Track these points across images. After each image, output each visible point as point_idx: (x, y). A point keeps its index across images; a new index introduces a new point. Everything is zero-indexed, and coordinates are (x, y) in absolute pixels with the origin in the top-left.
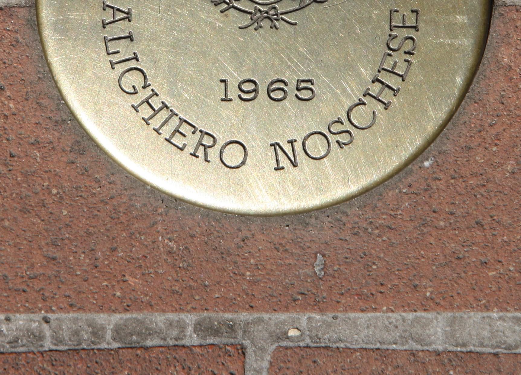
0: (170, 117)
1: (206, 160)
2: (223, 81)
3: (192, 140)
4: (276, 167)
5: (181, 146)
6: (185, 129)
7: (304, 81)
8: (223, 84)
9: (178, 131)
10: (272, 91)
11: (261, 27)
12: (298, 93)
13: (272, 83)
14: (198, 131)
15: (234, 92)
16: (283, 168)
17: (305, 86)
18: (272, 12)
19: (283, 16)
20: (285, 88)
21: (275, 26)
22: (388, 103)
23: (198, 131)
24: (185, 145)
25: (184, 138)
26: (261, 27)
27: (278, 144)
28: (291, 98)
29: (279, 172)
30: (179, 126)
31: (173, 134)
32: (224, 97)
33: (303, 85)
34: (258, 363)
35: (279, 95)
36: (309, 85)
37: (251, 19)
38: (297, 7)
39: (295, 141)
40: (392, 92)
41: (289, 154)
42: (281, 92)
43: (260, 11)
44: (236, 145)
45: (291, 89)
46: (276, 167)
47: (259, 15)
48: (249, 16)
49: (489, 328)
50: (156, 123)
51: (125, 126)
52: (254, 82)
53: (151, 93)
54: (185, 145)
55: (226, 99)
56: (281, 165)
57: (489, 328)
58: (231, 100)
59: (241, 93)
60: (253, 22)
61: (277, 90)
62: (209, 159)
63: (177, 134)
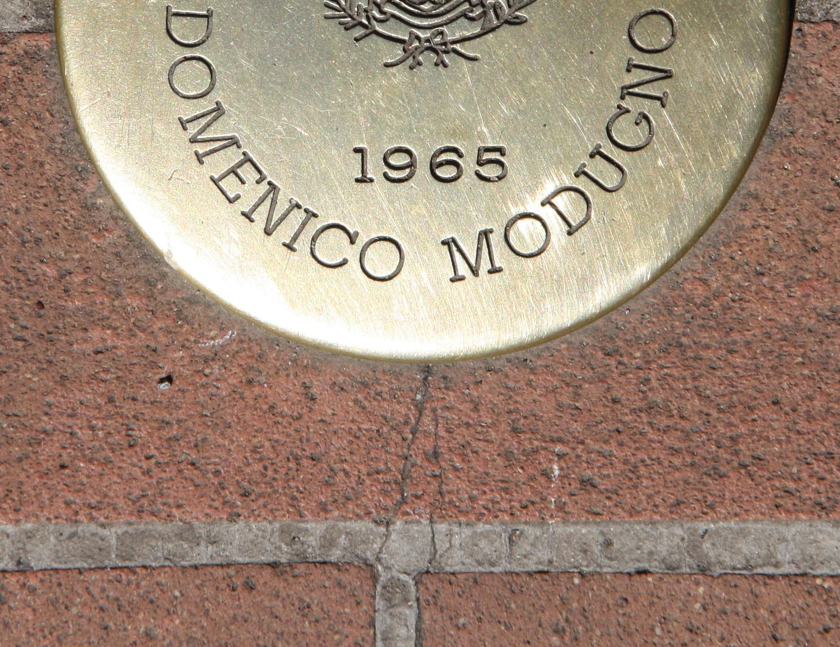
2: (357, 150)
5: (231, 196)
8: (359, 156)
10: (441, 165)
11: (419, 64)
12: (478, 168)
13: (435, 156)
17: (492, 157)
18: (438, 39)
19: (458, 47)
21: (443, 62)
24: (238, 197)
26: (419, 64)
27: (454, 241)
28: (468, 178)
30: (240, 165)
32: (360, 176)
35: (447, 172)
36: (496, 156)
37: (404, 50)
38: (478, 30)
43: (418, 38)
45: (469, 164)
47: (416, 44)
48: (401, 46)
49: (805, 541)
50: (284, 233)
52: (408, 152)
54: (238, 197)
57: (805, 541)
59: (387, 170)
60: (407, 55)
61: (444, 165)
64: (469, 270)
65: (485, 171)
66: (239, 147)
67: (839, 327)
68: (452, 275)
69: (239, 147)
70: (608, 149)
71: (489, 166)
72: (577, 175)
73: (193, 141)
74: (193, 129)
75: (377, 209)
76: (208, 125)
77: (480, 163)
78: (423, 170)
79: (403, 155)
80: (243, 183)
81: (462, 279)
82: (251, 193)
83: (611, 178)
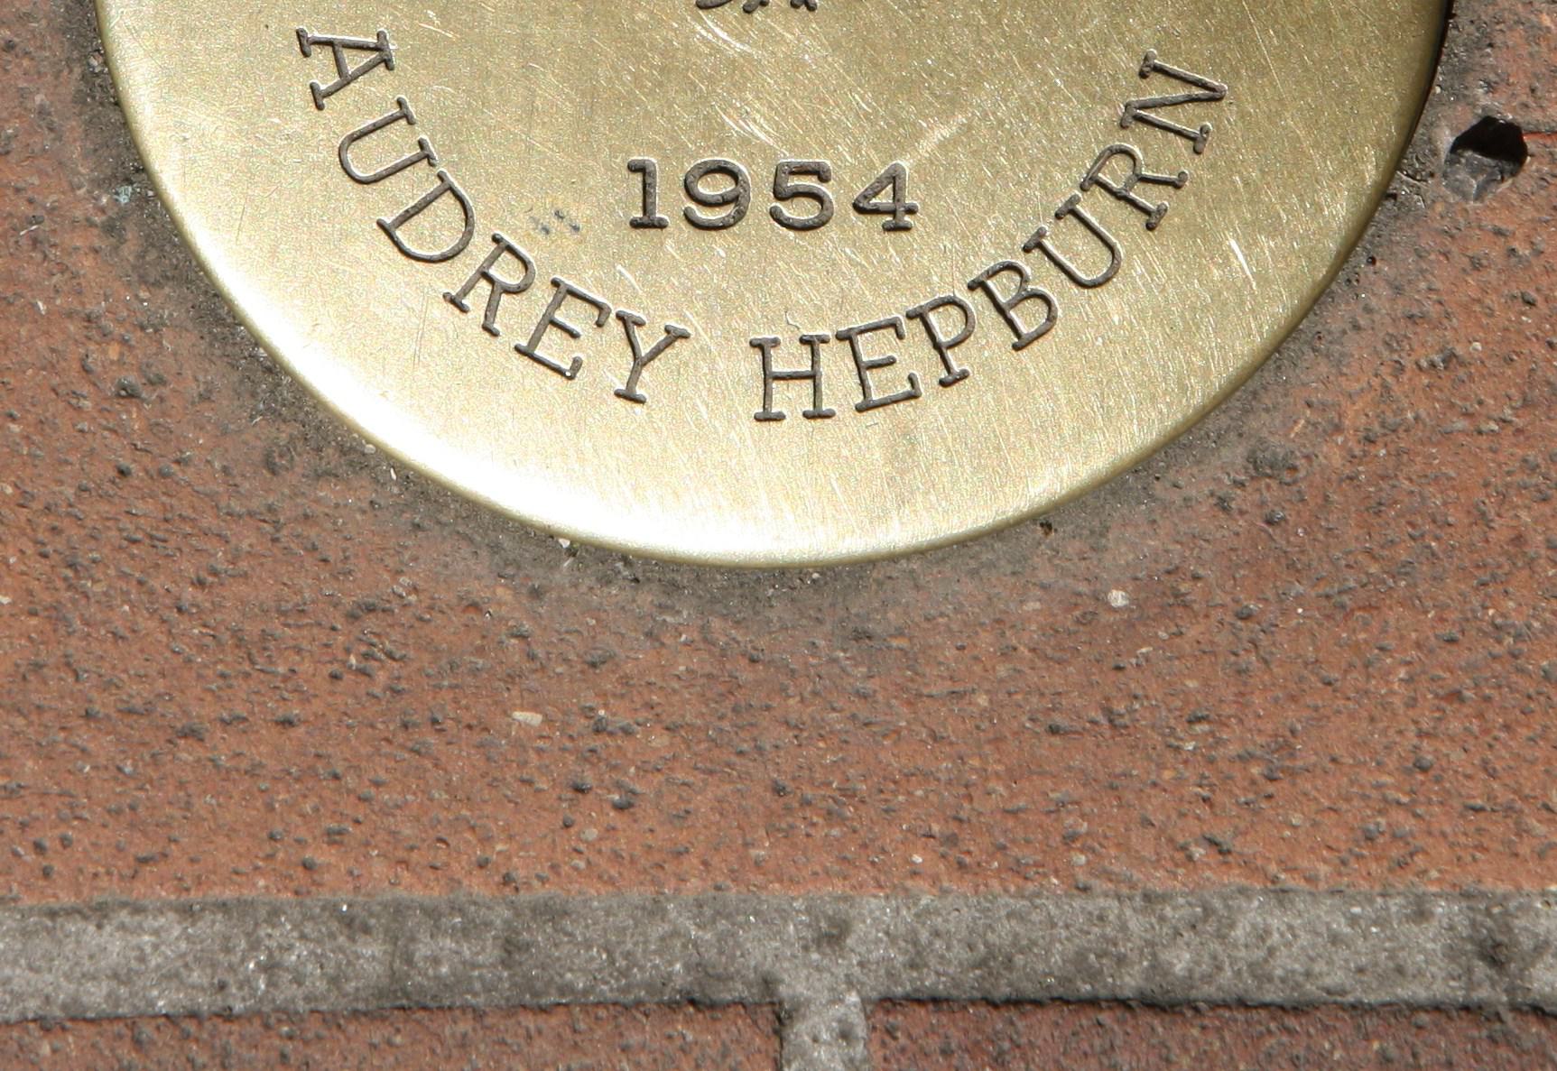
0: (394, 119)
2: (636, 168)
3: (914, 357)
5: (566, 365)
6: (570, 314)
7: (803, 171)
8: (638, 177)
14: (613, 315)
20: (823, 188)
22: (1159, 211)
23: (613, 315)
25: (572, 341)
29: (621, 402)
30: (493, 259)
32: (639, 215)
34: (829, 1014)
52: (733, 174)
55: (648, 223)
56: (825, 407)
58: (661, 225)
59: (693, 206)
62: (497, 326)
65: (723, 186)
68: (859, 399)
69: (824, 341)
75: (675, 278)
78: (758, 178)
79: (806, 202)
80: (890, 362)
82: (607, 359)
83: (1088, 261)
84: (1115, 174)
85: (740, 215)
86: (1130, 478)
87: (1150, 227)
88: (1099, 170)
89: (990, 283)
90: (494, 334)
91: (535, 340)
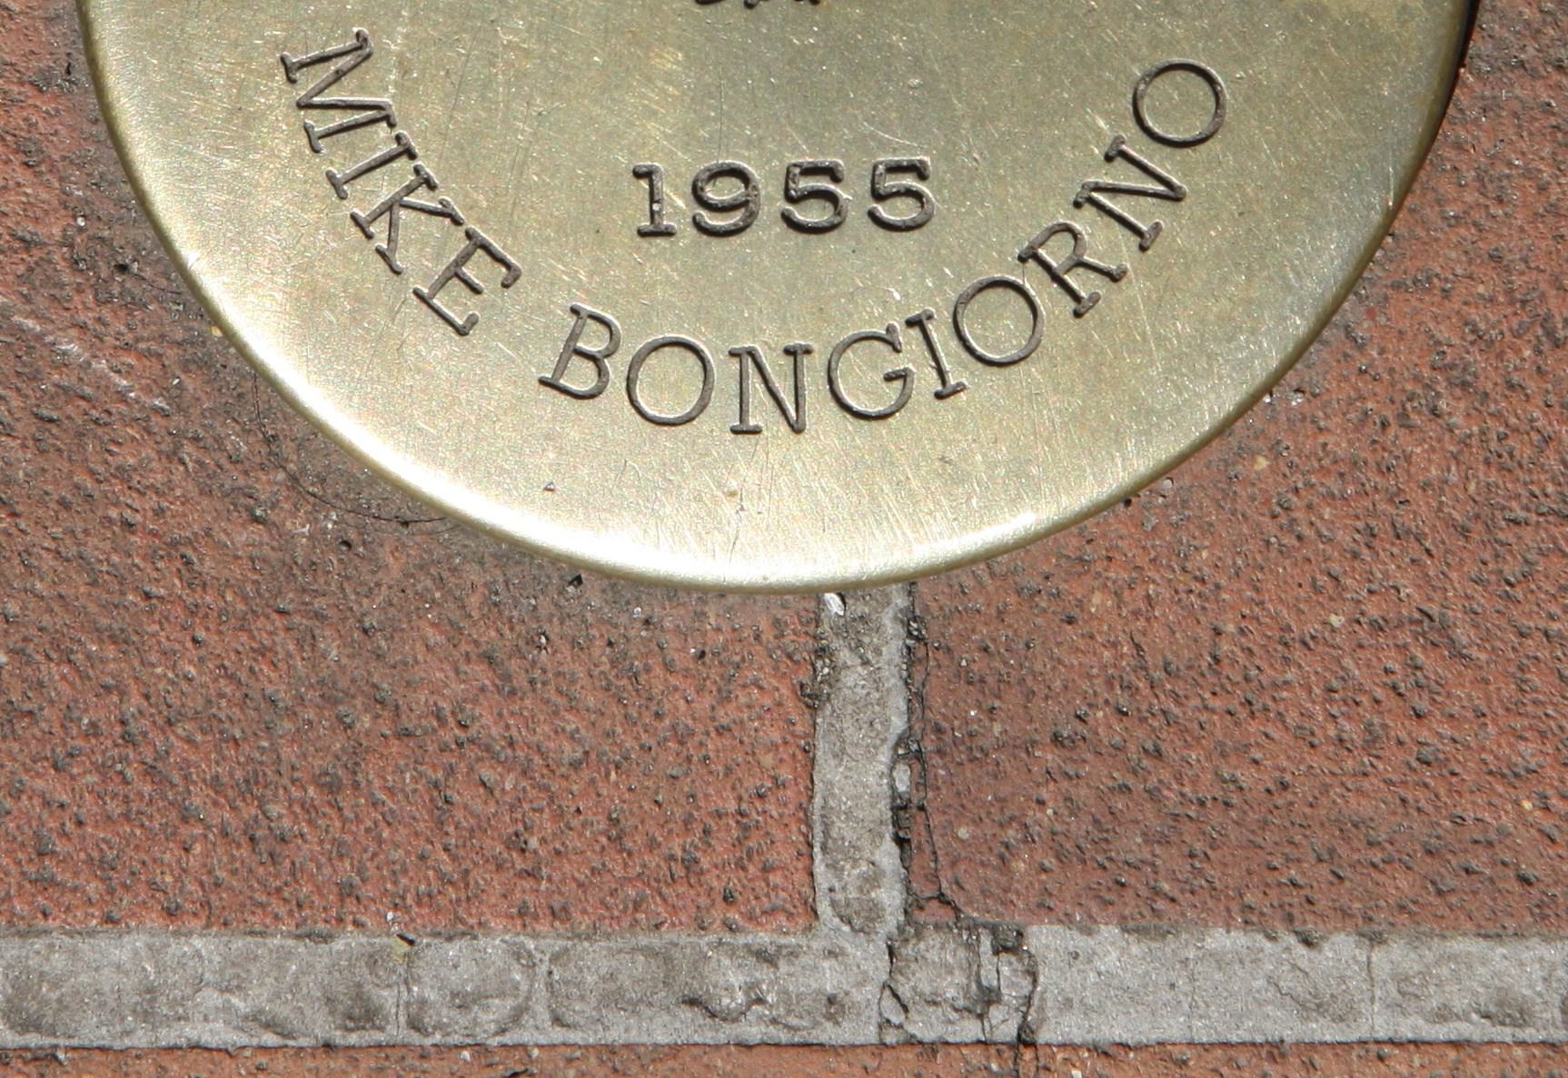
1: (1113, 277)
4: (940, 388)
5: (460, 322)
7: (896, 169)
8: (644, 184)
9: (457, 275)
15: (677, 203)
16: (756, 431)
20: (922, 187)
24: (472, 321)
27: (751, 353)
30: (465, 258)
31: (442, 284)
33: (806, 183)
35: (721, 192)
39: (808, 351)
40: (1135, 240)
41: (760, 387)
42: (911, 201)
44: (1000, 290)
46: (940, 388)
49: (1526, 966)
51: (1333, 156)
53: (395, 146)
54: (472, 321)
56: (752, 422)
63: (455, 281)
64: (1169, 203)
66: (391, 125)
67: (1566, 561)
70: (940, 333)
71: (813, 202)
72: (1022, 259)
73: (305, 106)
74: (308, 82)
76: (339, 75)
77: (878, 196)
80: (476, 290)
81: (1095, 299)
84: (1055, 254)
85: (752, 215)
86: (833, 601)
87: (1077, 314)
88: (1041, 245)
89: (1042, 252)
90: (638, 175)
91: (561, 368)
